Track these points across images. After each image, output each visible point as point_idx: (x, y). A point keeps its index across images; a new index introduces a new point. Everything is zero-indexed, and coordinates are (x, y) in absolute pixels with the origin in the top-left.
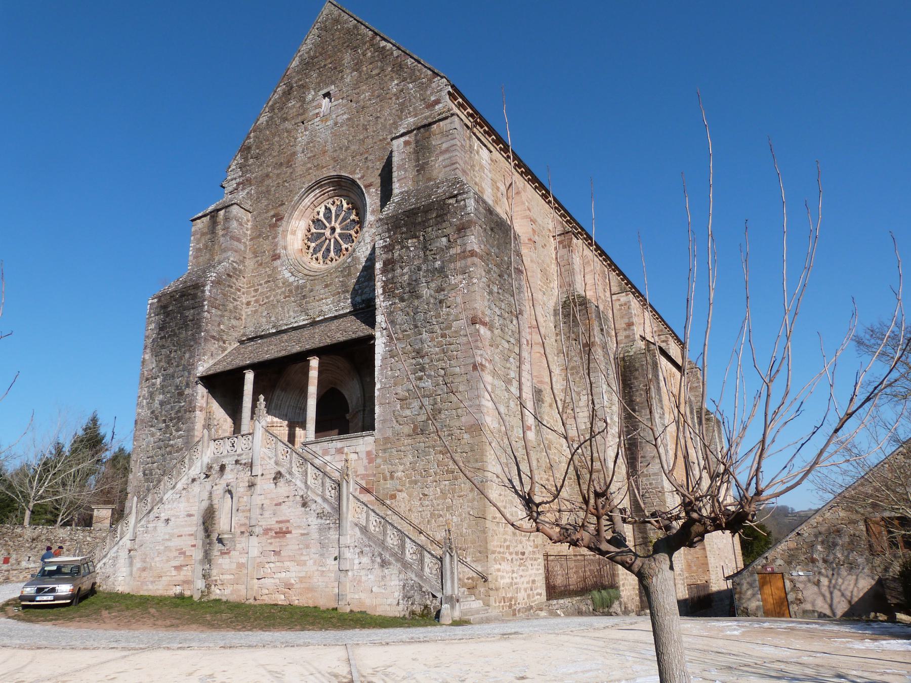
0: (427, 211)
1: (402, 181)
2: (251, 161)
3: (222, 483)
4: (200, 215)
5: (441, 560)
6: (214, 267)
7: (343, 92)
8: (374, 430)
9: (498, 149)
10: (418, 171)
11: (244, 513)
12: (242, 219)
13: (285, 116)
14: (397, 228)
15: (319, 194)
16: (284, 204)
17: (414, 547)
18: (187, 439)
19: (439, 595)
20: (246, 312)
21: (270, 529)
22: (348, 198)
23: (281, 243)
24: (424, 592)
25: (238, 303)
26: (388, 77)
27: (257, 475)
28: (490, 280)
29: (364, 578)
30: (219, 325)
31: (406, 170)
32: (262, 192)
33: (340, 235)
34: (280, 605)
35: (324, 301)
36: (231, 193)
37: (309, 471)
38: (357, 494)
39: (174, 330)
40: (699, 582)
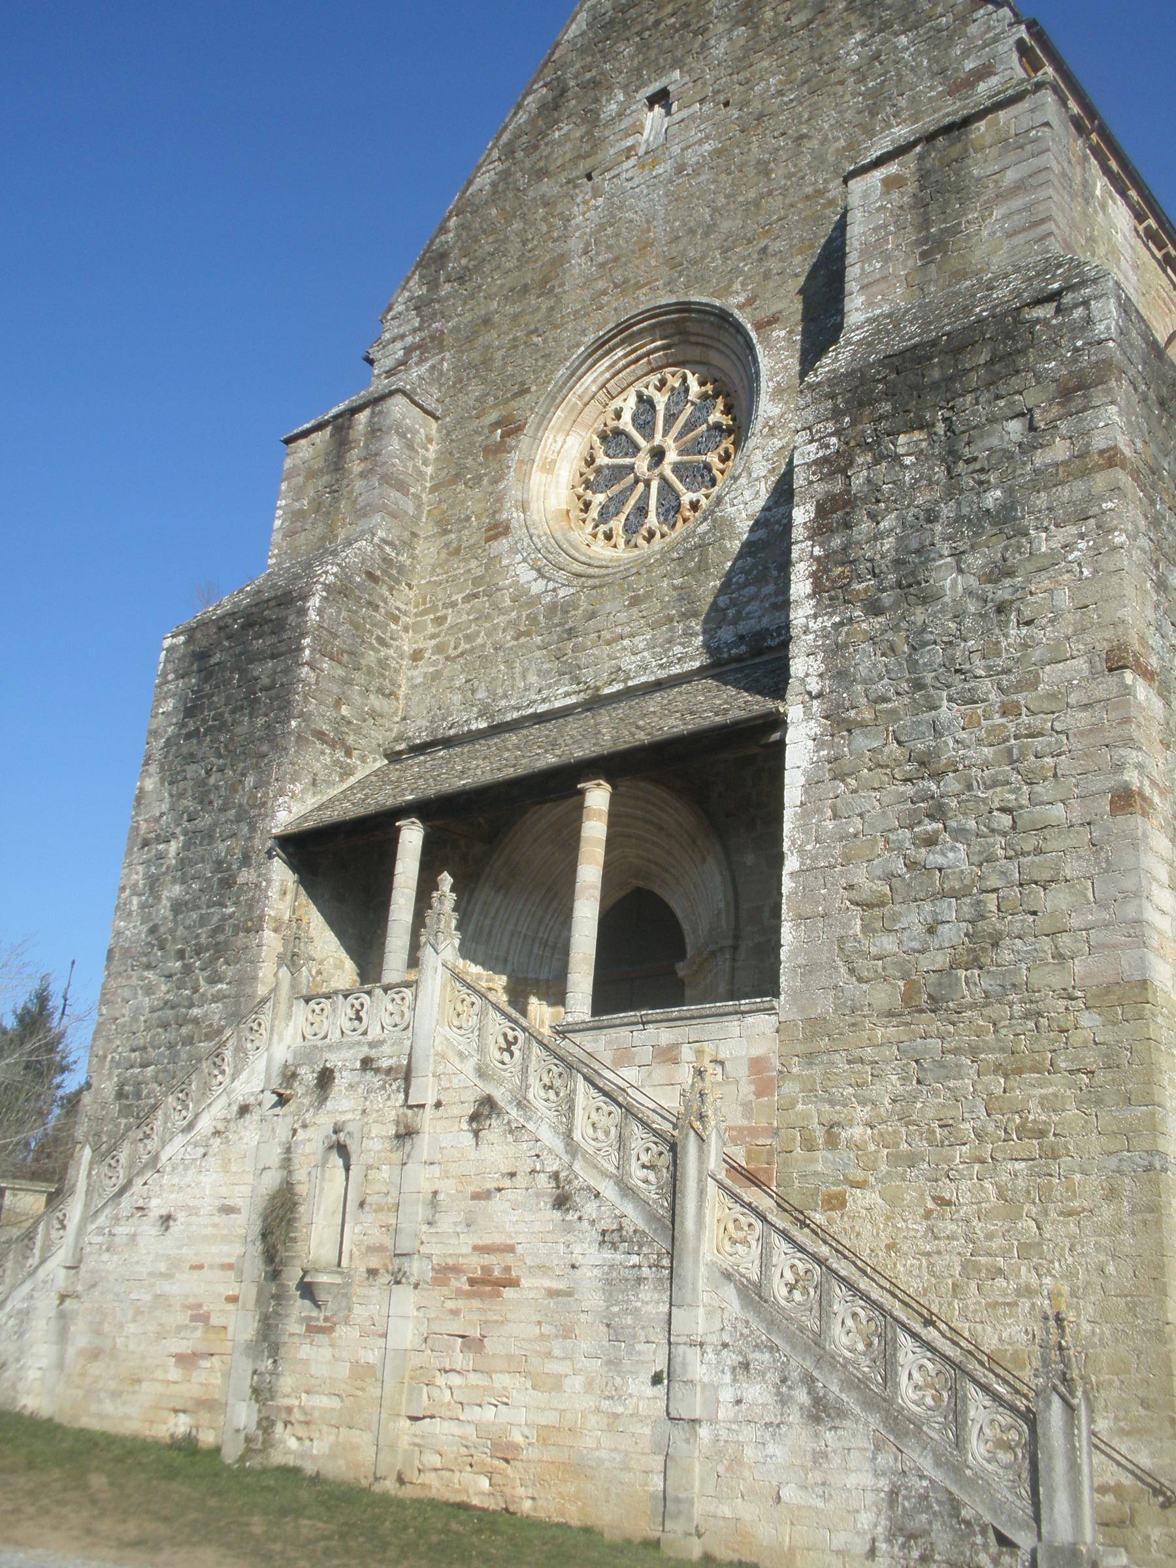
0: (960, 349)
1: (875, 289)
3: (324, 1121)
4: (307, 426)
5: (1031, 1419)
6: (335, 553)
7: (704, 84)
8: (776, 994)
9: (1142, 233)
10: (923, 255)
11: (380, 1216)
12: (415, 432)
13: (542, 164)
14: (861, 405)
15: (624, 362)
16: (528, 390)
17: (930, 1365)
18: (237, 1003)
19: (1024, 1540)
20: (410, 679)
21: (456, 1270)
22: (703, 369)
23: (515, 493)
24: (968, 1523)
25: (391, 652)
26: (836, 27)
27: (423, 1106)
28: (1159, 548)
29: (750, 1453)
30: (338, 704)
31: (887, 258)
32: (470, 366)
33: (677, 468)
34: (475, 1507)
35: (626, 642)
36: (390, 373)
37: (580, 1101)
38: (722, 1176)
39: (221, 715)
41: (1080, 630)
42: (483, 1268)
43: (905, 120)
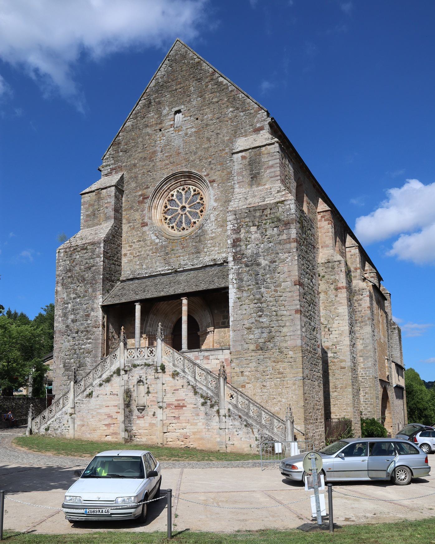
1: (240, 184)
2: (121, 154)
10: (252, 178)
16: (149, 187)
21: (172, 404)
23: (147, 215)
41: (289, 276)
42: (178, 404)
43: (243, 136)
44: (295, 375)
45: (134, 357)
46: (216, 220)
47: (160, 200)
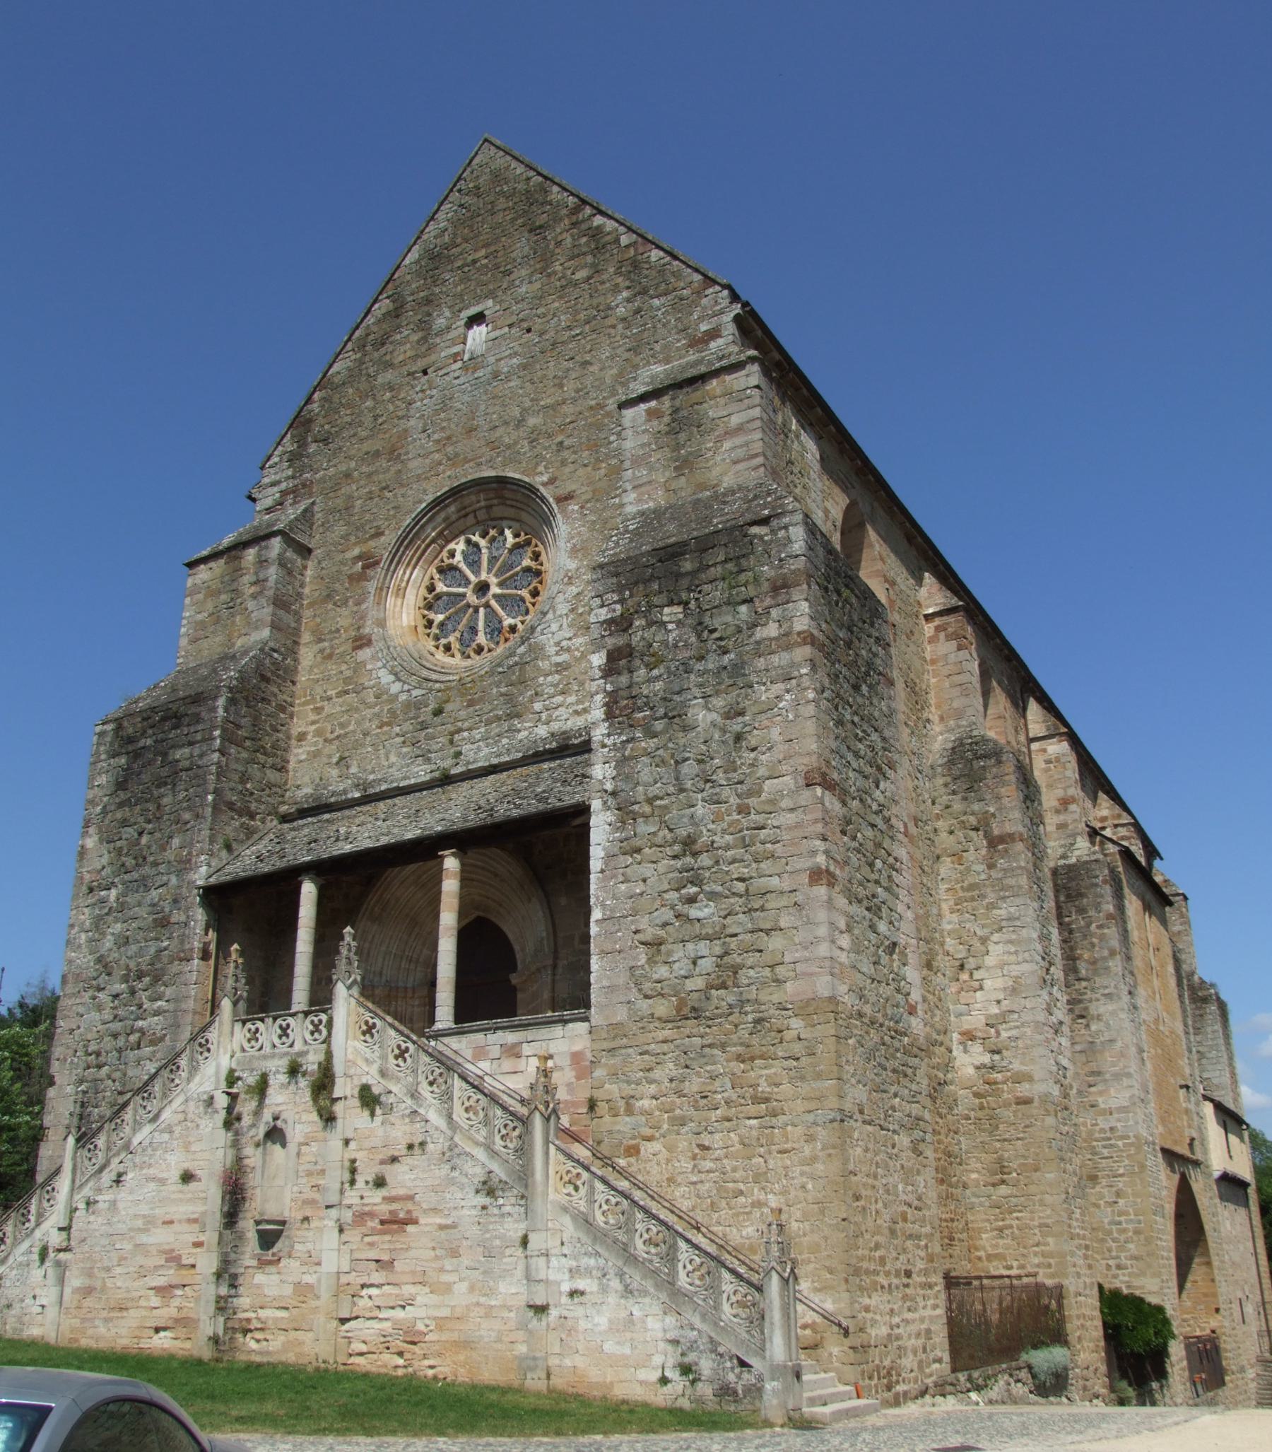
1: (643, 489)
4: (205, 553)
10: (676, 468)
16: (382, 534)
18: (176, 1017)
21: (371, 1215)
23: (373, 614)
24: (721, 1355)
25: (280, 735)
35: (466, 734)
36: (269, 510)
40: (1198, 1333)
42: (390, 1212)
44: (812, 1106)
45: (261, 1048)
46: (572, 610)
47: (414, 568)
